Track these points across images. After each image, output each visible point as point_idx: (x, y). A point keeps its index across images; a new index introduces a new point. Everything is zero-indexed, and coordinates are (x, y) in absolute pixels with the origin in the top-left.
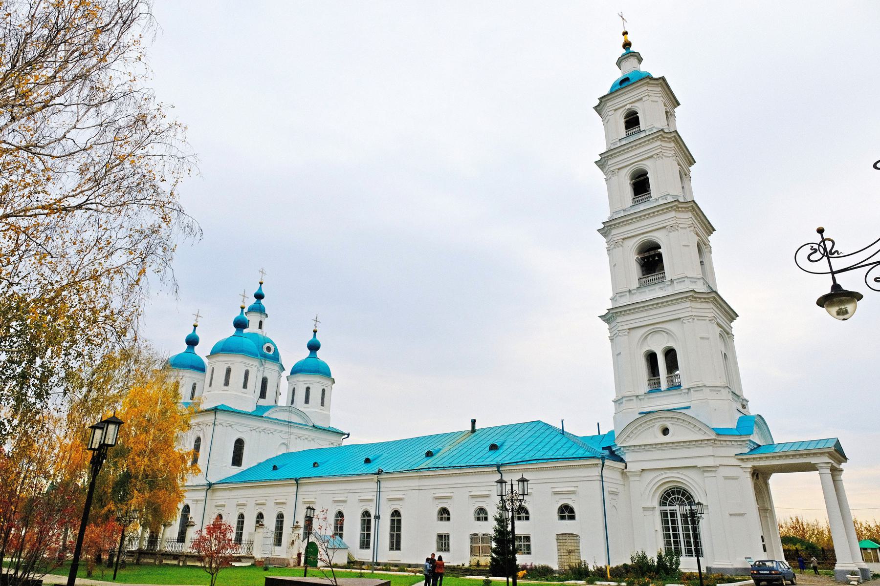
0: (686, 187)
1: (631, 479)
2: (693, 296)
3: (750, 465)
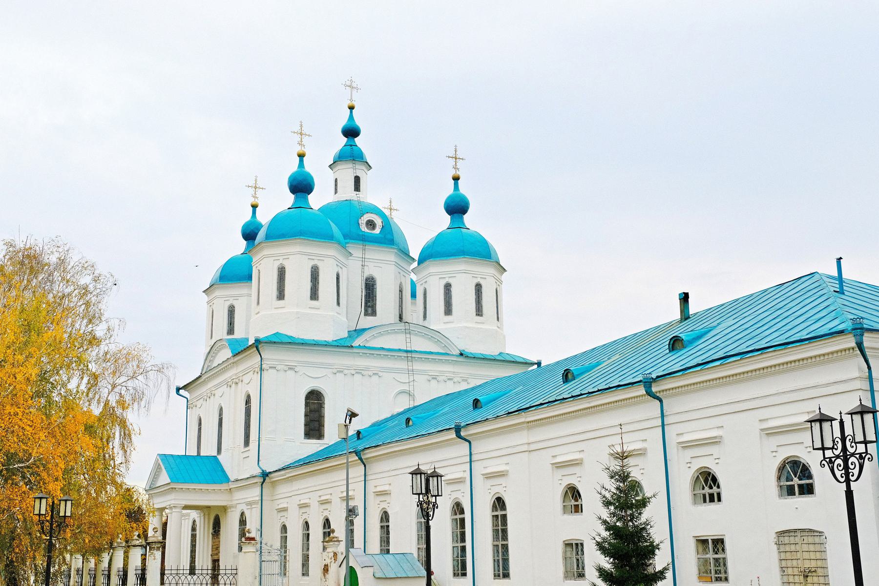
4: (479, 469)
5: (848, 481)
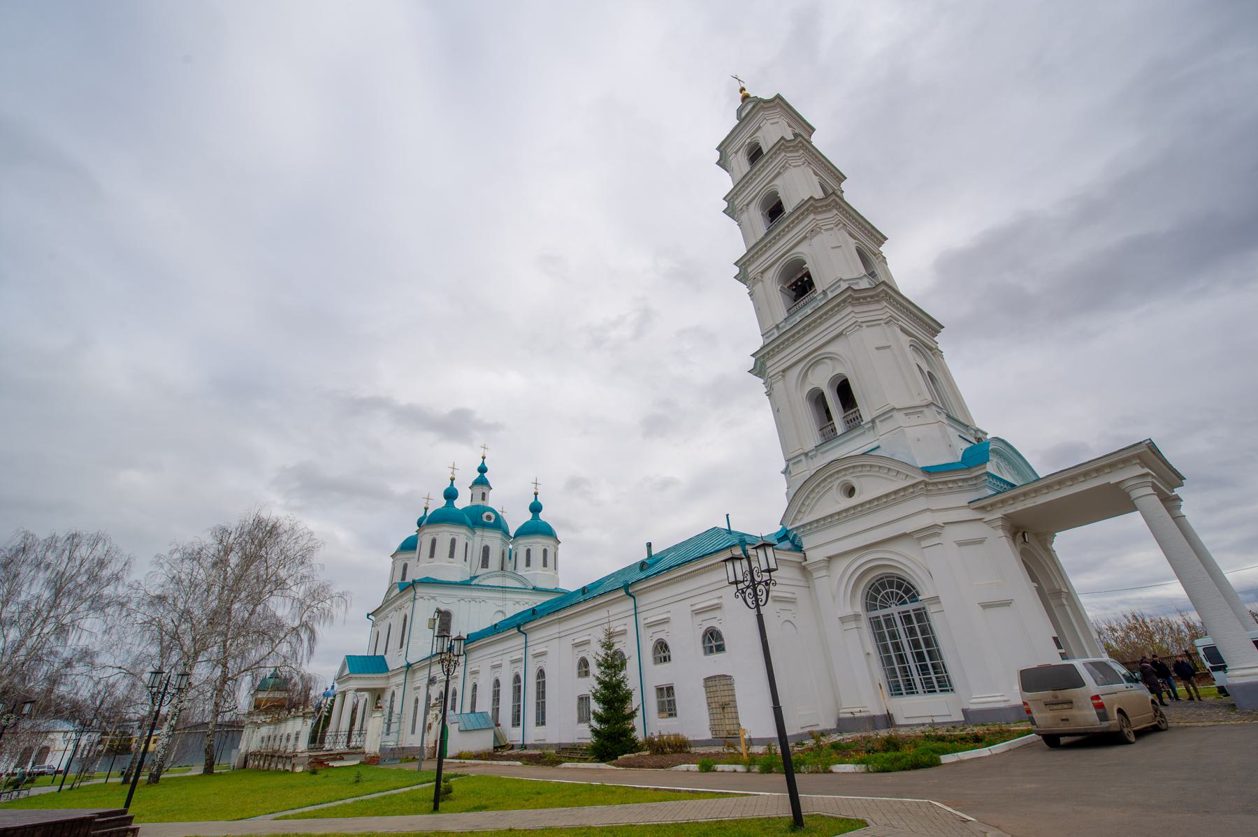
1: (816, 575)
2: (853, 297)
3: (998, 514)
4: (531, 651)
5: (758, 606)
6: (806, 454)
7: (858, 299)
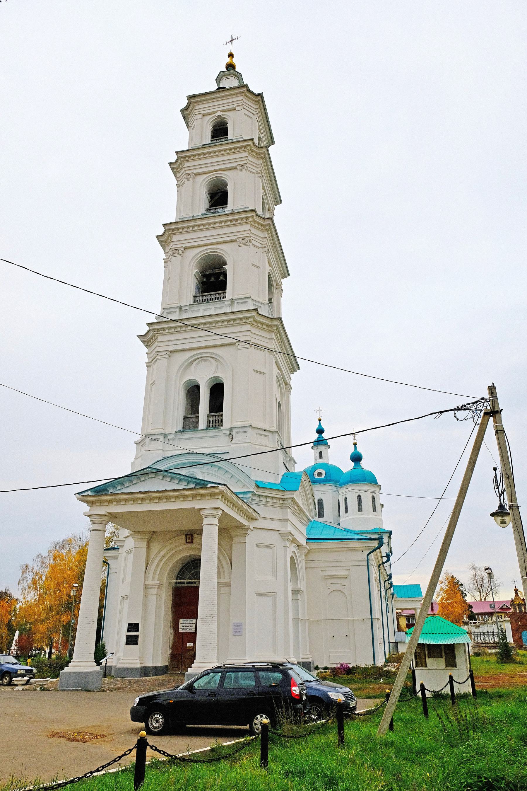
0: (274, 300)
6: (165, 435)
7: (257, 322)
